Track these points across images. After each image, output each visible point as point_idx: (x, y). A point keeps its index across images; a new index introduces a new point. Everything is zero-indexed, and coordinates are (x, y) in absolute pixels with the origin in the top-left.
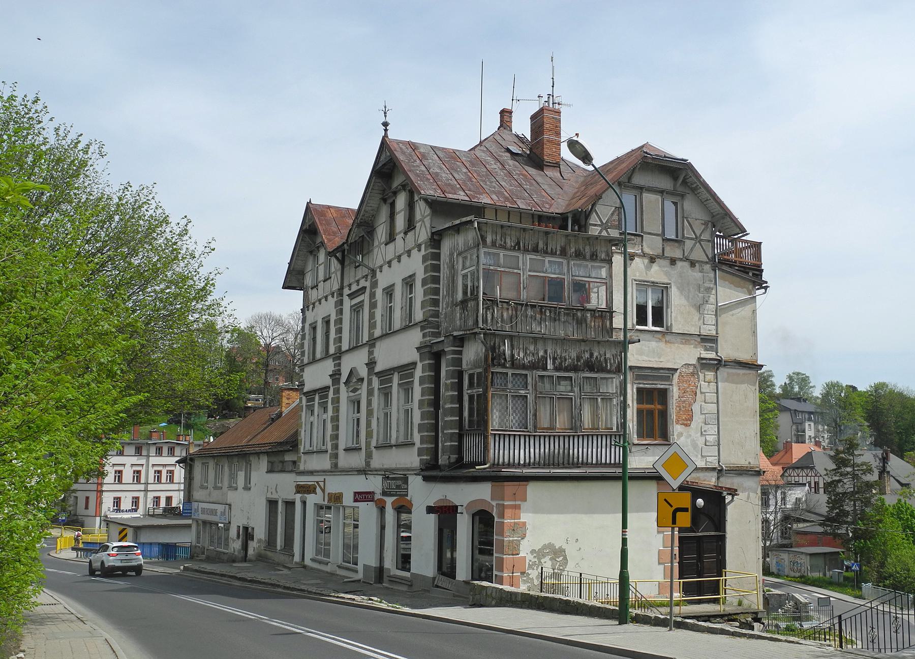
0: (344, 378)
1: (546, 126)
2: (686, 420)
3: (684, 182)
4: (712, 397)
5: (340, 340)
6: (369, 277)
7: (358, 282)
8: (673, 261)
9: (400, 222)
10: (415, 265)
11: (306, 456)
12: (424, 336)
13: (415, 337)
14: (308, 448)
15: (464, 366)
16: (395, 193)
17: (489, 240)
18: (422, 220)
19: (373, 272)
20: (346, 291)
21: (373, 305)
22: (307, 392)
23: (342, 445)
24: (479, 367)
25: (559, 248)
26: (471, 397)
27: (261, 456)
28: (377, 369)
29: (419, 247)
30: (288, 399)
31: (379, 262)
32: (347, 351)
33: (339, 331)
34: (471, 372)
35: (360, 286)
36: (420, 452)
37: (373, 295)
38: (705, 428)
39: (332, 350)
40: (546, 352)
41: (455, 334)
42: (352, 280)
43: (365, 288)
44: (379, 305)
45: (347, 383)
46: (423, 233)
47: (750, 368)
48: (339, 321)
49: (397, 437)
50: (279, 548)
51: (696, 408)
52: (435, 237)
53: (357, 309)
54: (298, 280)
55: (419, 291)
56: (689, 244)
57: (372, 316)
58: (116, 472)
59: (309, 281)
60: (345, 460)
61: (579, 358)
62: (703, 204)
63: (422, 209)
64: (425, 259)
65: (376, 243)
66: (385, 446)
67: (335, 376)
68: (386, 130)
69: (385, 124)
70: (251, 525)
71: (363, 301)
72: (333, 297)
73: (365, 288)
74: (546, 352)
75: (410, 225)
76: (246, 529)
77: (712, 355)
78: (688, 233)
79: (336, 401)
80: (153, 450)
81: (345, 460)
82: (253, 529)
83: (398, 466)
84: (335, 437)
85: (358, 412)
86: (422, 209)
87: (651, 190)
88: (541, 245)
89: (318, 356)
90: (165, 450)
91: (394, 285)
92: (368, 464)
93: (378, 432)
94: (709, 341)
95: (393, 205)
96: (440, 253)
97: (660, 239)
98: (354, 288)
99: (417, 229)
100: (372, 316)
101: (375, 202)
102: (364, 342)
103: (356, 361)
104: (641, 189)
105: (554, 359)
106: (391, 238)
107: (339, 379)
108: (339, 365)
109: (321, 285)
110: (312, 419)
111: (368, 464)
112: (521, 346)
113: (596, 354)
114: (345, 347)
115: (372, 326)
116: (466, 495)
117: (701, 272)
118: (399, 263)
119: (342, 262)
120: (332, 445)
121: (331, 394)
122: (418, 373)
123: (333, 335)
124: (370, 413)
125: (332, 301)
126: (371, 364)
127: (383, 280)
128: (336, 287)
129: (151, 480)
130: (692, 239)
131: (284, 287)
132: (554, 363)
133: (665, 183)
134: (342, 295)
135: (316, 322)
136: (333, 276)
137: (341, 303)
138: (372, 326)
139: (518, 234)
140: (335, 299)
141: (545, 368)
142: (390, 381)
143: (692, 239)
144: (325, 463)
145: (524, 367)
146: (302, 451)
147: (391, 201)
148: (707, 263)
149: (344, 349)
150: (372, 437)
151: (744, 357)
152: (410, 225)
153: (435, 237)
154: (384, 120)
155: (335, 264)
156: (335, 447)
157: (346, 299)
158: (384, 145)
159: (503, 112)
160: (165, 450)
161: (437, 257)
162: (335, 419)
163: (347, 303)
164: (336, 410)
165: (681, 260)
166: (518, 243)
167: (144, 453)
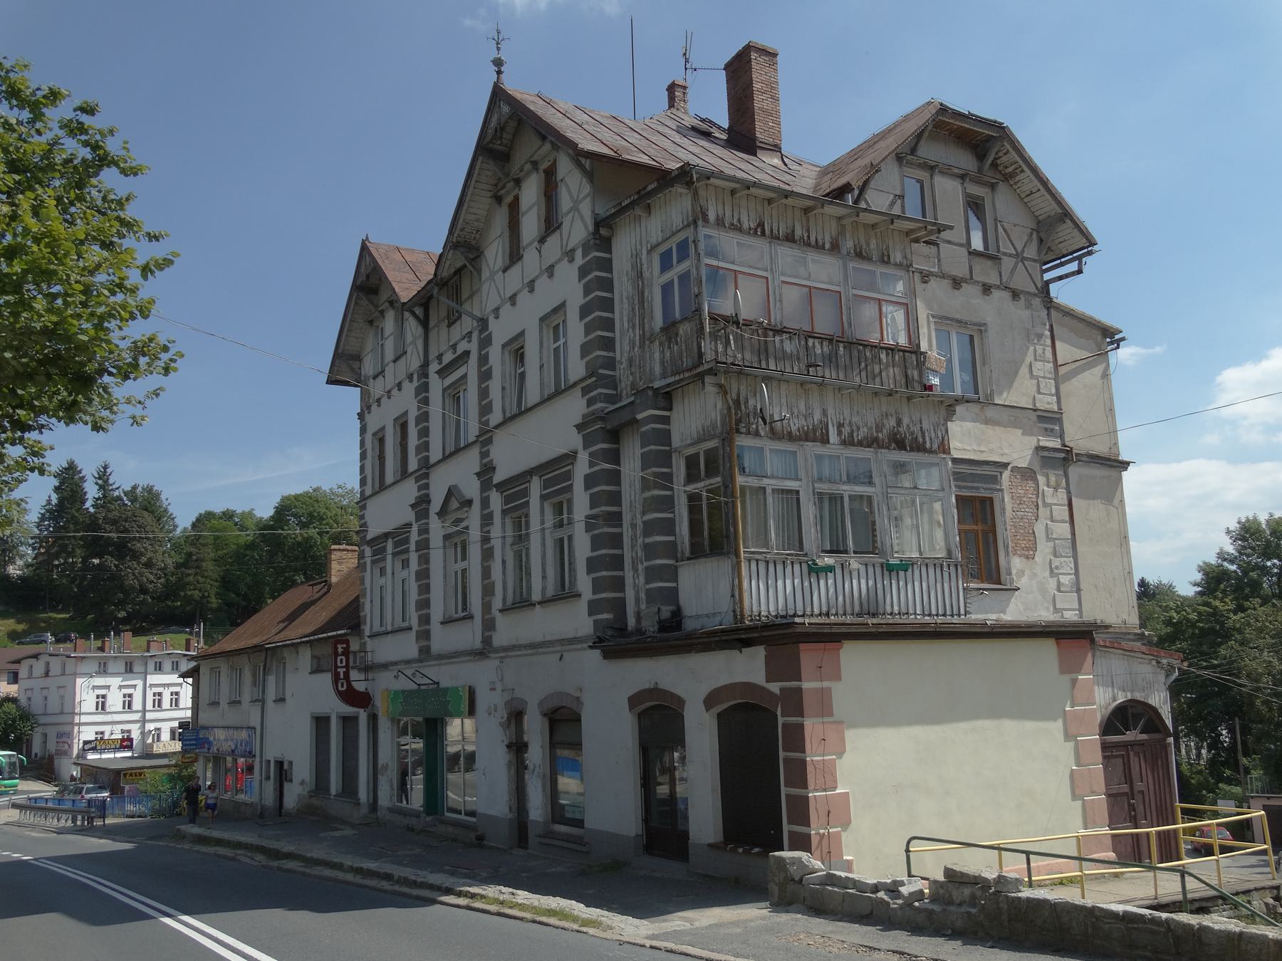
0: (435, 506)
1: (756, 86)
2: (1028, 549)
3: (994, 165)
4: (1062, 512)
5: (424, 447)
6: (475, 336)
7: (454, 347)
8: (987, 289)
9: (530, 226)
10: (568, 287)
11: (376, 641)
12: (590, 403)
13: (574, 407)
14: (377, 628)
15: (676, 441)
16: (518, 182)
17: (712, 216)
18: (575, 208)
19: (483, 323)
20: (435, 366)
21: (485, 376)
22: (373, 540)
23: (437, 613)
24: (711, 438)
25: (828, 239)
26: (693, 499)
27: (301, 649)
28: (498, 478)
29: (570, 255)
30: (340, 563)
31: (491, 306)
32: (439, 462)
33: (424, 432)
34: (691, 451)
35: (459, 352)
36: (594, 607)
37: (483, 359)
38: (1056, 562)
39: (413, 465)
40: (824, 413)
41: (657, 384)
42: (443, 348)
43: (467, 353)
44: (497, 373)
45: (442, 513)
46: (577, 230)
47: (1111, 466)
48: (424, 417)
49: (544, 589)
50: (333, 791)
51: (1039, 529)
52: (603, 231)
53: (454, 395)
54: (352, 370)
55: (576, 332)
56: (1007, 263)
57: (484, 393)
58: (98, 697)
59: (368, 367)
60: (442, 639)
61: (879, 428)
62: (1024, 200)
63: (573, 184)
64: (583, 272)
65: (485, 273)
66: (522, 603)
67: (420, 507)
68: (499, 73)
69: (498, 63)
70: (287, 758)
71: (465, 376)
72: (411, 381)
73: (467, 353)
74: (824, 413)
75: (551, 224)
76: (280, 764)
77: (1054, 443)
78: (1006, 247)
79: (423, 545)
80: (151, 666)
81: (442, 639)
82: (291, 763)
83: (548, 638)
84: (424, 604)
85: (464, 558)
86: (573, 184)
87: (947, 171)
88: (798, 232)
89: (389, 478)
90: (167, 665)
91: (522, 333)
92: (487, 641)
93: (505, 583)
94: (1050, 420)
95: (514, 207)
96: (610, 260)
97: (964, 251)
98: (448, 358)
99: (565, 227)
100: (484, 393)
101: (481, 203)
102: (471, 439)
103: (461, 474)
104: (931, 168)
105: (840, 426)
106: (515, 256)
107: (427, 510)
108: (427, 486)
109: (389, 370)
110: (382, 581)
111: (487, 641)
112: (784, 401)
113: (906, 421)
114: (435, 454)
115: (485, 410)
116: (695, 679)
117: (1027, 308)
118: (533, 295)
119: (425, 323)
120: (420, 617)
121: (414, 537)
122: (582, 468)
123: (413, 440)
124: (487, 554)
125: (410, 388)
126: (486, 471)
127: (501, 331)
128: (414, 362)
129: (149, 706)
130: (1010, 255)
131: (330, 382)
132: (840, 433)
133: (963, 160)
134: (426, 376)
135: (383, 428)
136: (409, 350)
137: (424, 388)
138: (485, 410)
139: (759, 208)
140: (415, 383)
141: (825, 440)
142: (525, 493)
143: (1010, 255)
144: (407, 647)
145: (791, 437)
146: (367, 633)
147: (509, 199)
148: (1035, 295)
149: (433, 460)
150: (493, 594)
151: (1100, 448)
152: (551, 224)
153: (603, 231)
154: (495, 55)
155: (412, 328)
156: (425, 620)
157: (434, 380)
158: (498, 94)
159: (672, 88)
160: (167, 665)
161: (607, 265)
162: (423, 575)
163: (436, 386)
164: (424, 560)
165: (998, 287)
166: (761, 225)
167: (137, 668)
